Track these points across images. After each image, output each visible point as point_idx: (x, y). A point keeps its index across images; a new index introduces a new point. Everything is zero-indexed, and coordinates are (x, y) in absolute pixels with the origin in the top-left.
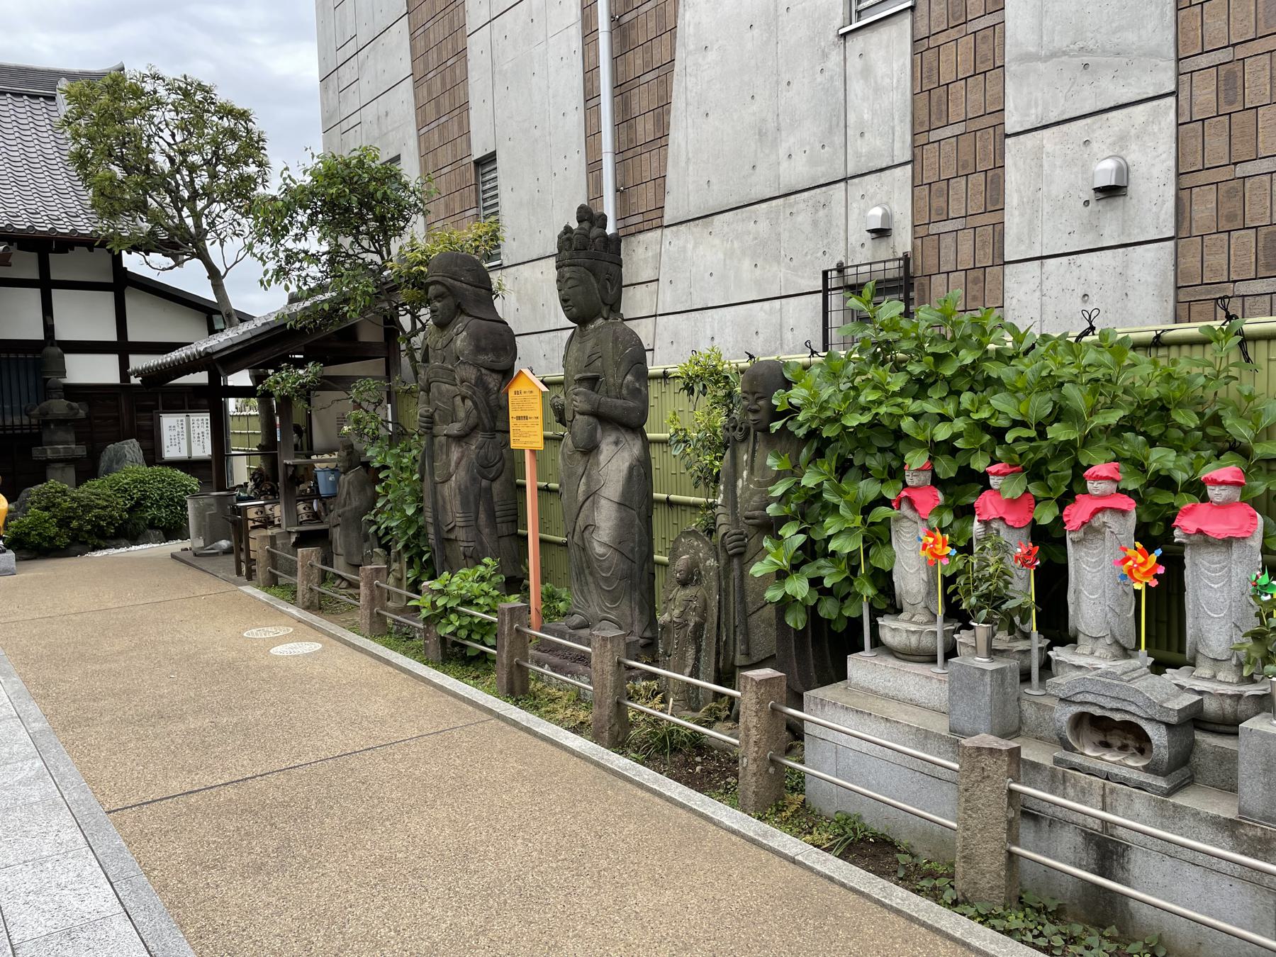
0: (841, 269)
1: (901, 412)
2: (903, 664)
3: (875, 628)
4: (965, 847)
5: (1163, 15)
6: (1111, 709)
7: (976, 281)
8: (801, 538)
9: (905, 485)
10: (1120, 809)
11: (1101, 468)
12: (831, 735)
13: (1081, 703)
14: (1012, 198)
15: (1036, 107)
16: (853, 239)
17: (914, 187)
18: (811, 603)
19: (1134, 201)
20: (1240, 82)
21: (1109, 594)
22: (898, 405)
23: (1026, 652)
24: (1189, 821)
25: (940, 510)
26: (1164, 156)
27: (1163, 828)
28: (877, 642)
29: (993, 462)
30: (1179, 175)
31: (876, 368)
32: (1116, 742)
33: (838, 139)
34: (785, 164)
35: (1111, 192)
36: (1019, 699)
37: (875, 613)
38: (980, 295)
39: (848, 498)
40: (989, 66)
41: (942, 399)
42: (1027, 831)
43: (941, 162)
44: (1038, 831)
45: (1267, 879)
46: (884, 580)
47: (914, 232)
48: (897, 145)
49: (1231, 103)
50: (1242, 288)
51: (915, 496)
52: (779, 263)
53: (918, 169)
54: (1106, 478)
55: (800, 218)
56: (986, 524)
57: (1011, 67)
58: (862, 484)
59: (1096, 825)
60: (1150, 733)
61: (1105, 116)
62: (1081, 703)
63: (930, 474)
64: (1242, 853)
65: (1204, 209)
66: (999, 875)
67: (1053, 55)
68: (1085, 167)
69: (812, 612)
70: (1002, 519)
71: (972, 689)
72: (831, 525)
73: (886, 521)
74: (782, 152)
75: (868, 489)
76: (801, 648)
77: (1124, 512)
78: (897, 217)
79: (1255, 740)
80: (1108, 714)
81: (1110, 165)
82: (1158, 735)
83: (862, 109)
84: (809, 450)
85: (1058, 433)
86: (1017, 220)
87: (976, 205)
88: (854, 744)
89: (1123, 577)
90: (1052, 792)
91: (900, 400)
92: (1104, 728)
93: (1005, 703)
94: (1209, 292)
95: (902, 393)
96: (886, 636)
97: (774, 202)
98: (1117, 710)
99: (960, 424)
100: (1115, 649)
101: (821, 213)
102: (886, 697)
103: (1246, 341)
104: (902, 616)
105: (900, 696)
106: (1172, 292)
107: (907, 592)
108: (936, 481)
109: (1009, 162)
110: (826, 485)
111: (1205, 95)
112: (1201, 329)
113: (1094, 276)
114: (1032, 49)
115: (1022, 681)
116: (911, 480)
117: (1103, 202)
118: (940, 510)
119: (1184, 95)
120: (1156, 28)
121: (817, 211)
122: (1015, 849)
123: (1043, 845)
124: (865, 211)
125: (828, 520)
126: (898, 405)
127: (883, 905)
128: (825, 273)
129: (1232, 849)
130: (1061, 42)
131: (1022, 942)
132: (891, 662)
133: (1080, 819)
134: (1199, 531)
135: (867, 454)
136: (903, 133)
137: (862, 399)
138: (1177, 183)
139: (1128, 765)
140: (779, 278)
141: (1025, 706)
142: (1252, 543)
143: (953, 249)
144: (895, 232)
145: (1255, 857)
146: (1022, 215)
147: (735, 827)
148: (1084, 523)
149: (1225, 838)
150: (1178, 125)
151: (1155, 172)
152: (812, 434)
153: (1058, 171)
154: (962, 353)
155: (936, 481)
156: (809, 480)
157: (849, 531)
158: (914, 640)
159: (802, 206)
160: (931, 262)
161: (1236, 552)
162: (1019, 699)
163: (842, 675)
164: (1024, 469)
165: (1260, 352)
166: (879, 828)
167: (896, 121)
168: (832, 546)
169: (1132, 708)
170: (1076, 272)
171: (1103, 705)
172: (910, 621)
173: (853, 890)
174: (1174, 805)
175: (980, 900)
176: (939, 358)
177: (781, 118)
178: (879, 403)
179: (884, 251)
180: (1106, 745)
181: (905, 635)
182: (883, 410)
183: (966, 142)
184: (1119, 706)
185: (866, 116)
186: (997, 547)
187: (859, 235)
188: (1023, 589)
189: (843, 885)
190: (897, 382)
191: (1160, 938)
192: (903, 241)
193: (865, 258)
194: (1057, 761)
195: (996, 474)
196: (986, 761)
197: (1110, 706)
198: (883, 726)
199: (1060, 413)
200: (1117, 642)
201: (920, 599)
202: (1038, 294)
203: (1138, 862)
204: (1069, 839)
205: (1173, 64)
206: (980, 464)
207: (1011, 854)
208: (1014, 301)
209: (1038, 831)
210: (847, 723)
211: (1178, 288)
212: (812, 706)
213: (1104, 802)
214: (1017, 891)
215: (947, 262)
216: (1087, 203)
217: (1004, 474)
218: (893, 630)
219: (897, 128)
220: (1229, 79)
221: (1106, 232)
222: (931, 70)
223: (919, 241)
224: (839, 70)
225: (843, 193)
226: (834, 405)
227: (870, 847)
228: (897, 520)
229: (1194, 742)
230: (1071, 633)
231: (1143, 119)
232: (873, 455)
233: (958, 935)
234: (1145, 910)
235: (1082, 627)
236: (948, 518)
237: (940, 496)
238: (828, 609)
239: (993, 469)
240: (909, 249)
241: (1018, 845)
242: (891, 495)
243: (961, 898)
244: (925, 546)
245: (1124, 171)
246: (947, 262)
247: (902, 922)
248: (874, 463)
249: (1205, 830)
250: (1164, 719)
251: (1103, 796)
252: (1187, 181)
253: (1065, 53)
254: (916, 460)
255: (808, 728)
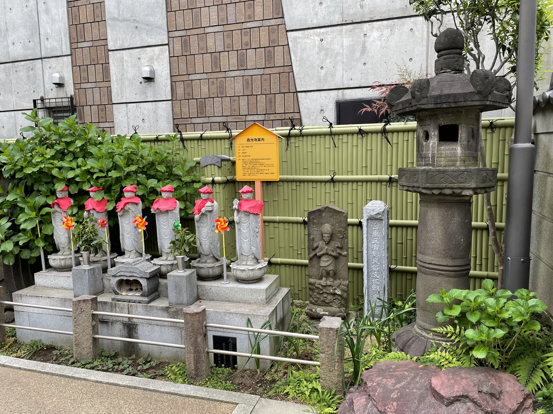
0: (42, 99)
1: (53, 166)
2: (59, 273)
3: (47, 260)
4: (76, 340)
5: (162, 13)
6: (129, 276)
7: (102, 110)
8: (9, 224)
9: (57, 198)
10: (134, 312)
11: (129, 188)
12: (26, 309)
13: (120, 276)
14: (113, 78)
15: (120, 40)
16: (47, 86)
17: (73, 66)
18: (16, 253)
19: (157, 84)
20: (189, 44)
21: (133, 234)
22: (51, 164)
23: (106, 260)
24: (155, 311)
25: (72, 207)
26: (166, 68)
27: (147, 315)
28: (48, 266)
29: (92, 186)
30: (171, 76)
31: (40, 147)
32: (134, 288)
33: (37, 40)
34: (11, 47)
35: (149, 79)
36: (102, 279)
37: (46, 253)
38: (104, 116)
39: (29, 204)
40: (99, 19)
41: (71, 161)
42: (101, 328)
43: (84, 57)
44: (108, 327)
45: (178, 324)
46: (49, 239)
47: (74, 87)
48: (64, 47)
49: (186, 52)
50: (194, 121)
51: (61, 202)
52: (12, 94)
53: (74, 57)
54: (130, 191)
55: (21, 74)
56: (89, 211)
57: (108, 22)
58: (37, 198)
59: (127, 320)
60: (141, 283)
61: (145, 49)
62: (120, 276)
63: (67, 192)
64: (171, 318)
65: (180, 91)
66: (90, 348)
67: (124, 20)
68: (139, 69)
69: (17, 257)
70: (94, 209)
71: (81, 278)
72: (22, 218)
73: (48, 214)
74: (10, 40)
75: (40, 200)
76: (17, 274)
77: (136, 204)
78: (66, 79)
79: (172, 278)
80: (128, 278)
81: (147, 69)
82: (144, 282)
83: (46, 28)
84: (12, 184)
85: (114, 174)
86: (116, 86)
87: (100, 78)
88: (36, 310)
89: (135, 227)
90: (112, 312)
91: (52, 161)
92: (130, 284)
93: (95, 281)
94: (184, 121)
95: (53, 158)
96: (51, 263)
97: (7, 65)
98: (131, 276)
99: (78, 171)
100: (137, 254)
101: (31, 72)
102: (52, 288)
103: (182, 140)
104: (59, 253)
105: (58, 287)
106: (172, 120)
107: (61, 243)
108: (70, 196)
109: (111, 61)
110: (19, 199)
111: (178, 47)
112: (166, 135)
113: (146, 112)
114: (116, 16)
115: (103, 273)
116: (59, 195)
117: (147, 83)
118: (72, 207)
119: (171, 46)
120: (159, 18)
121: (29, 71)
122: (96, 336)
123: (110, 332)
124: (52, 74)
125: (21, 215)
126: (51, 164)
127: (41, 372)
128: (35, 101)
129: (168, 317)
130: (127, 16)
131: (98, 370)
132: (55, 273)
133: (121, 319)
134: (158, 209)
135: (40, 185)
136: (66, 41)
137: (34, 161)
138: (171, 80)
139: (134, 295)
140: (13, 102)
141: (105, 281)
142: (175, 212)
143: (92, 95)
144: (66, 85)
145: (174, 318)
146: (118, 84)
147: (112, 381)
148: (122, 209)
149: (166, 314)
150: (170, 57)
151: (163, 74)
152: (13, 177)
153: (130, 68)
154: (77, 141)
155: (70, 196)
156: (10, 198)
157: (31, 219)
158: (63, 263)
159: (21, 68)
160: (83, 100)
161: (170, 215)
162: (102, 279)
163: (33, 283)
164: (103, 189)
165: (188, 144)
166: (48, 343)
167: (62, 36)
168: (22, 227)
169: (135, 275)
170: (139, 110)
171: (127, 275)
172: (62, 255)
173: (29, 370)
174: (150, 306)
175: (83, 359)
176: (68, 144)
177: (8, 25)
178: (41, 162)
179: (61, 93)
180: (131, 290)
181: (59, 261)
182: (43, 166)
183: (93, 50)
184: (131, 275)
185: (48, 31)
186: (92, 220)
187: (50, 86)
188: (104, 236)
189: (25, 369)
190: (50, 153)
191: (149, 355)
192: (70, 90)
193: (55, 97)
194: (113, 299)
195: (92, 191)
196: (83, 305)
197: (128, 275)
198: (47, 301)
199: (116, 167)
200: (137, 252)
201: (66, 245)
202: (126, 117)
203: (142, 330)
204: (118, 327)
205: (166, 33)
206: (86, 187)
207: (95, 339)
208: (118, 120)
209: (108, 327)
210: (32, 302)
211: (174, 119)
212: (17, 298)
213: (128, 311)
214: (99, 352)
215: (90, 101)
216: (141, 83)
217: (95, 191)
218: (54, 260)
219: (63, 39)
220: (185, 44)
221: (149, 95)
222: (76, 16)
223: (77, 90)
224: (35, 7)
225: (41, 65)
226: (20, 164)
227: (43, 352)
228: (53, 213)
229: (159, 283)
230: (122, 251)
231: (158, 53)
232: (42, 185)
233: (70, 375)
234: (105, 341)
235: (126, 248)
236: (75, 210)
237: (72, 201)
238: (26, 255)
239: (91, 189)
240: (73, 94)
241: (98, 334)
242: (50, 203)
243: (75, 361)
244: (64, 223)
245: (153, 72)
246: (90, 101)
247: (49, 376)
248: (43, 188)
249: (160, 313)
250: (145, 277)
251: (128, 309)
252: (174, 79)
253: (128, 20)
254: (59, 187)
255: (15, 308)
